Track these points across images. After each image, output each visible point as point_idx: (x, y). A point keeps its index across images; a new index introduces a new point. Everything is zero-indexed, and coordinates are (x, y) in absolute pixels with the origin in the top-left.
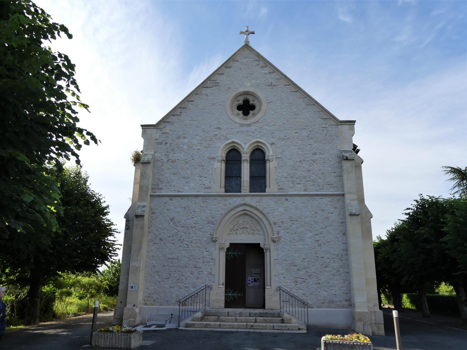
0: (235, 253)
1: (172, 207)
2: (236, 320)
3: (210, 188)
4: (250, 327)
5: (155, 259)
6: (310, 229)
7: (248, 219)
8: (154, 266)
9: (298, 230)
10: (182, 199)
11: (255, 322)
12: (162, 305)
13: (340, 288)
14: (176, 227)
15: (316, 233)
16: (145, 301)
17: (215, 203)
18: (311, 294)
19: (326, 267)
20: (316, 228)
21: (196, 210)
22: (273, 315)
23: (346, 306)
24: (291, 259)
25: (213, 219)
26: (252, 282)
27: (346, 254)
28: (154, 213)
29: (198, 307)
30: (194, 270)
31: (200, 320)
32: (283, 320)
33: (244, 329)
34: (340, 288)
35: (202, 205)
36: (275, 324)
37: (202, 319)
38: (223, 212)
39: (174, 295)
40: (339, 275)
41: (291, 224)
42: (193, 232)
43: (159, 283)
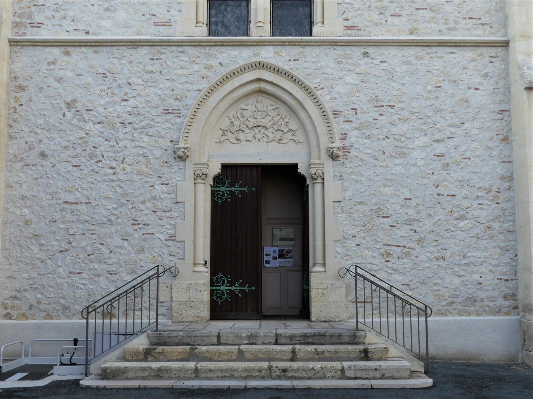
0: (236, 189)
1: (69, 74)
2: (241, 356)
3: (168, 24)
4: (278, 373)
5: (29, 203)
6: (424, 127)
7: (266, 104)
8: (28, 223)
9: (394, 130)
10: (95, 52)
11: (292, 360)
12: (51, 318)
13: (491, 267)
14: (82, 124)
15: (438, 136)
16: (6, 308)
17: (182, 64)
18: (423, 283)
19: (462, 218)
20: (438, 126)
21: (134, 80)
22: (337, 339)
23: (506, 310)
24: (374, 201)
25: (178, 103)
26: (275, 258)
27: (509, 188)
28: (22, 88)
29: (145, 321)
30: (130, 229)
31: (141, 356)
32: (366, 351)
33: (264, 378)
34: (491, 267)
35: (149, 68)
36: (346, 364)
37: (147, 355)
38: (205, 85)
39: (81, 293)
40: (491, 237)
41: (376, 115)
42: (128, 136)
43: (40, 265)
